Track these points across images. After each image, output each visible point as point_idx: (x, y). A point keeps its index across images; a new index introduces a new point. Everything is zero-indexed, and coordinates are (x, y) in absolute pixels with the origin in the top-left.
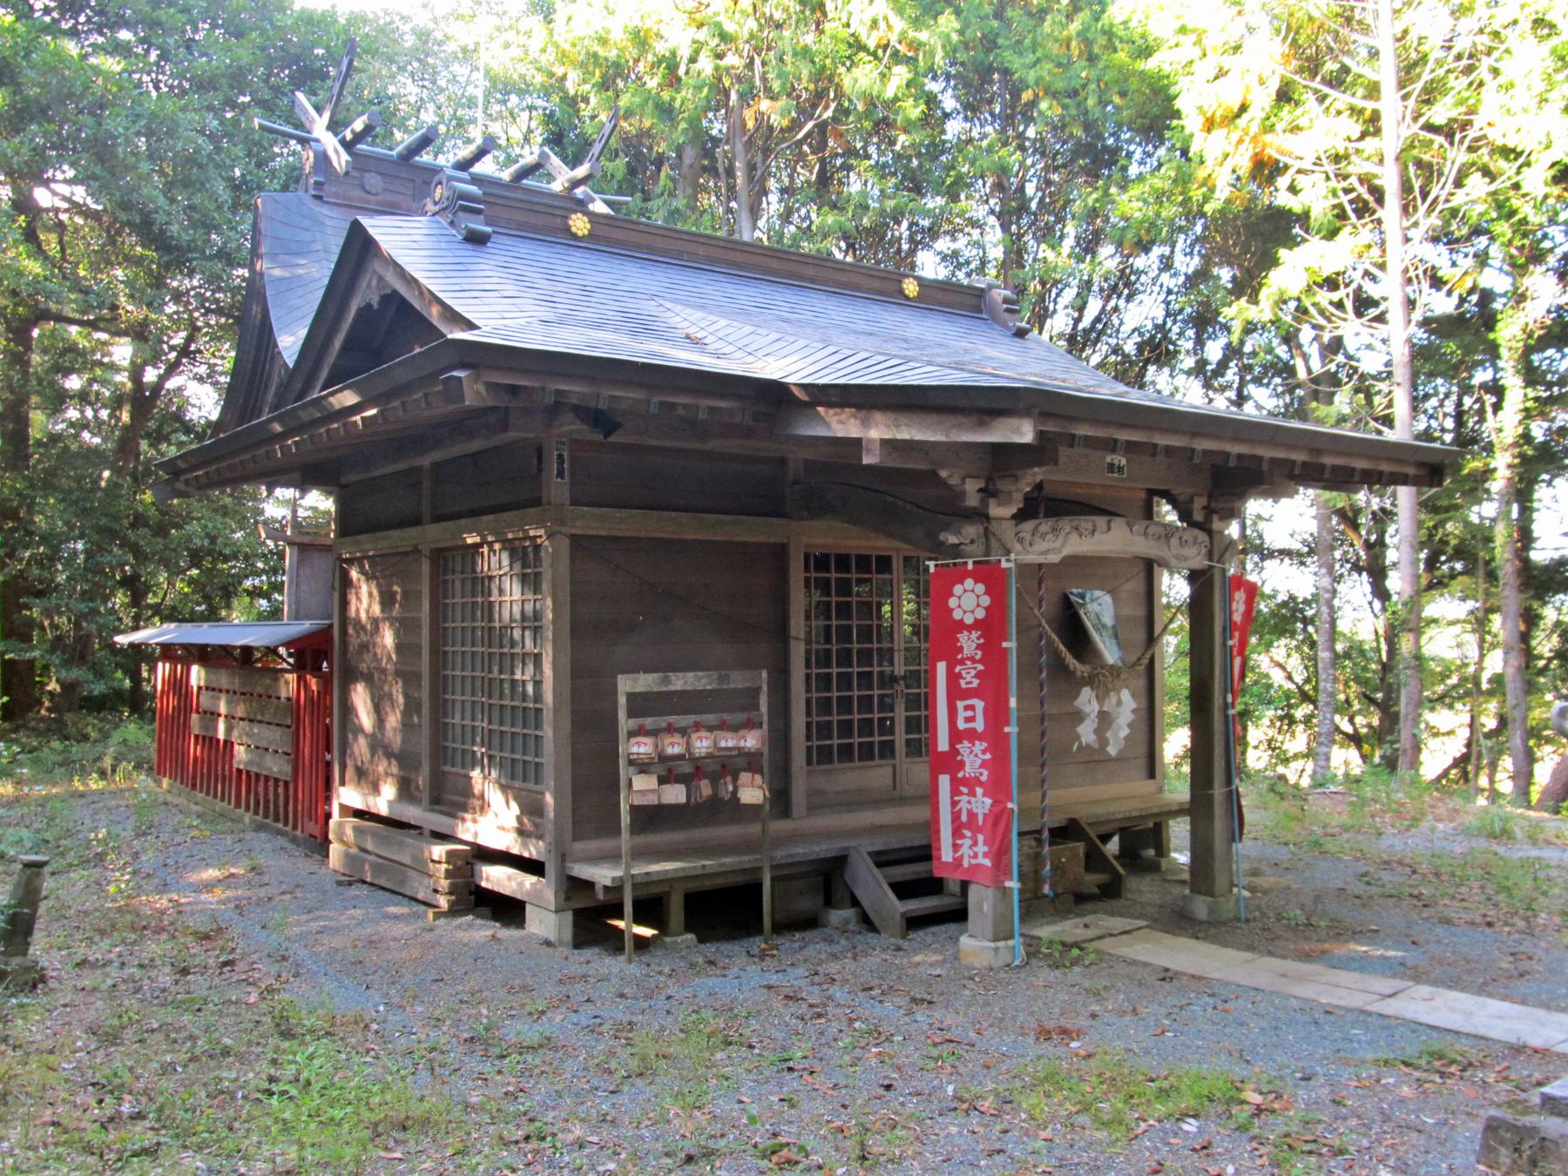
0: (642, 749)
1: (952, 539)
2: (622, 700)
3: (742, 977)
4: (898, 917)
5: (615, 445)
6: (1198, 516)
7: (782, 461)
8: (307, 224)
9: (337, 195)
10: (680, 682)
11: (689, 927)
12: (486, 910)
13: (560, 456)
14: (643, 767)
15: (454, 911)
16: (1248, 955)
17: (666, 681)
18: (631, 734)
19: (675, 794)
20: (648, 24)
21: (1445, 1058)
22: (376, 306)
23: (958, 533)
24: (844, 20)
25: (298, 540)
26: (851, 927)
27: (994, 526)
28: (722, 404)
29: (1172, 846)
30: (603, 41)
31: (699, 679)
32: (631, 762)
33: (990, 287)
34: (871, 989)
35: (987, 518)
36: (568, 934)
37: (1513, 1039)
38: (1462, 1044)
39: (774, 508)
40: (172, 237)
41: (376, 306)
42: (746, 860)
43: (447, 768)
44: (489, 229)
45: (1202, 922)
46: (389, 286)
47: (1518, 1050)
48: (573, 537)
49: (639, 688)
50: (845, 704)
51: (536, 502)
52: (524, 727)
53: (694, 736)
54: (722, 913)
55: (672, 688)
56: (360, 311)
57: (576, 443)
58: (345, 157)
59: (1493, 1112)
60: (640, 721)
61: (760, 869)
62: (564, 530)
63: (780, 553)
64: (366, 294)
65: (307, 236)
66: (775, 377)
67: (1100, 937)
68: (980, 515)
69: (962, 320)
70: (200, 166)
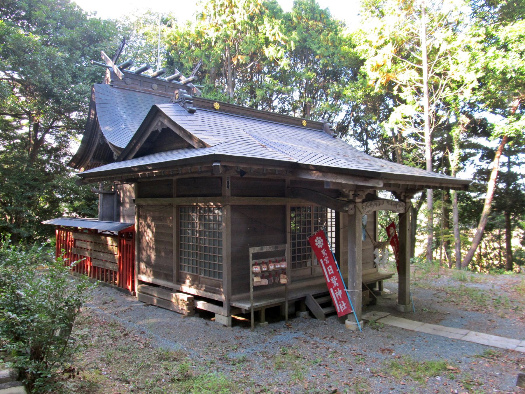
0: (257, 270)
1: (347, 209)
2: (251, 255)
3: (285, 336)
4: (323, 315)
5: (245, 178)
6: (402, 198)
7: (284, 181)
8: (109, 94)
9: (117, 85)
10: (266, 249)
11: (266, 320)
12: (198, 315)
13: (228, 182)
14: (256, 275)
15: (189, 315)
16: (421, 323)
17: (262, 249)
18: (253, 265)
19: (265, 282)
20: (202, 30)
21: (491, 354)
22: (160, 131)
23: (348, 207)
24: (264, 32)
25: (103, 192)
26: (307, 317)
27: (357, 205)
28: (281, 169)
29: (384, 286)
30: (189, 35)
31: (270, 248)
32: (253, 273)
33: (325, 123)
34: (326, 338)
35: (355, 203)
36: (230, 323)
37: (504, 348)
38: (493, 350)
39: (282, 195)
40: (54, 93)
41: (160, 131)
42: (281, 300)
43: (182, 271)
44: (195, 109)
45: (403, 312)
46: (166, 126)
47: (507, 351)
48: (232, 206)
49: (255, 252)
50: (299, 250)
51: (220, 195)
52: (205, 260)
53: (270, 265)
54: (273, 315)
55: (263, 251)
56: (153, 132)
57: (232, 178)
58: (121, 74)
59: (520, 372)
60: (255, 261)
61: (285, 302)
62: (229, 204)
63: (284, 207)
64: (156, 126)
65: (109, 98)
66: (295, 161)
67: (379, 319)
68: (353, 202)
69: (319, 133)
70: (61, 70)
